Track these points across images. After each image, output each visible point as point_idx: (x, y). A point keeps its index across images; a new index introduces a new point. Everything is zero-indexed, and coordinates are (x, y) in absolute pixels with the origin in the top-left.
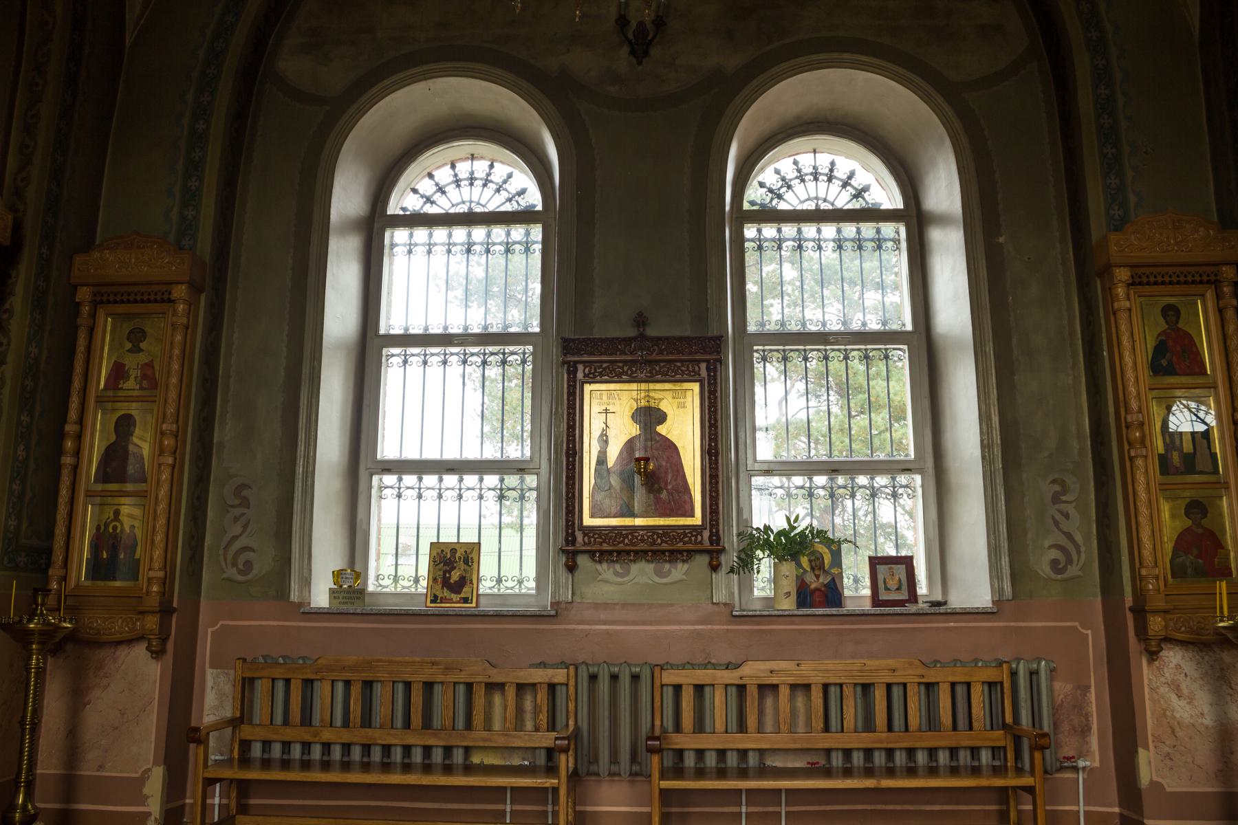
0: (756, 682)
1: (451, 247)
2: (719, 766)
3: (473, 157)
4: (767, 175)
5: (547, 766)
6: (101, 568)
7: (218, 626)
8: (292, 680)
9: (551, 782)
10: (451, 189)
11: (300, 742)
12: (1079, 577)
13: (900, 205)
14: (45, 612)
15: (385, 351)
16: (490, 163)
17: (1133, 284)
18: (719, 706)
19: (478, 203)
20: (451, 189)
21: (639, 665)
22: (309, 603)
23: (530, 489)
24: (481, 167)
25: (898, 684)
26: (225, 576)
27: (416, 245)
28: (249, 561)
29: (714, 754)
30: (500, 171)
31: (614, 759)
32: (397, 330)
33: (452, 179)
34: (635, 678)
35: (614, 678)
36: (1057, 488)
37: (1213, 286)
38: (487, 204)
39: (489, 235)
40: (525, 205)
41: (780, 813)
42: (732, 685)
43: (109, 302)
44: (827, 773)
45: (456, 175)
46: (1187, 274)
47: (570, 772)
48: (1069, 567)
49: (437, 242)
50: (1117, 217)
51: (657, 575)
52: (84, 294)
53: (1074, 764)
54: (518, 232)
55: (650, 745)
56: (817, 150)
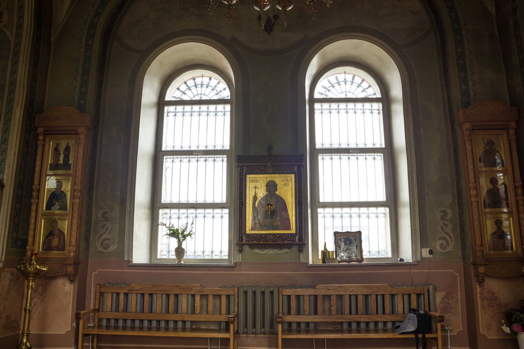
0: (149, 292)
1: (209, 113)
2: (307, 329)
3: (202, 76)
4: (323, 82)
5: (148, 327)
6: (48, 247)
7: (97, 271)
8: (412, 294)
9: (226, 335)
10: (193, 89)
11: (182, 321)
12: (452, 251)
13: (379, 95)
14: (35, 263)
15: (165, 157)
16: (353, 76)
17: (473, 130)
18: (307, 306)
19: (204, 95)
20: (193, 89)
21: (273, 287)
22: (132, 261)
23: (225, 214)
24: (206, 80)
25: (354, 295)
26: (98, 250)
27: (210, 112)
28: (106, 244)
29: (295, 324)
30: (214, 82)
31: (263, 326)
32: (170, 148)
33: (194, 84)
34: (272, 293)
35: (263, 293)
36: (443, 214)
37: (506, 130)
38: (208, 95)
39: (216, 108)
40: (223, 96)
41: (89, 346)
42: (311, 295)
43: (51, 134)
44: (342, 331)
45: (195, 83)
46: (495, 125)
47: (235, 332)
48: (448, 247)
49: (195, 111)
50: (465, 102)
51: (104, 250)
52: (40, 130)
53: (444, 328)
54: (220, 107)
55: (230, 319)
56: (346, 72)
